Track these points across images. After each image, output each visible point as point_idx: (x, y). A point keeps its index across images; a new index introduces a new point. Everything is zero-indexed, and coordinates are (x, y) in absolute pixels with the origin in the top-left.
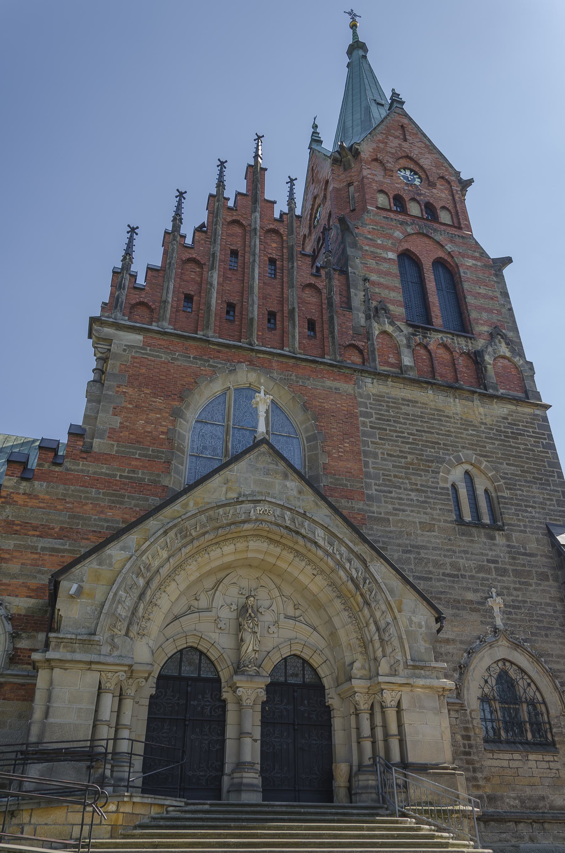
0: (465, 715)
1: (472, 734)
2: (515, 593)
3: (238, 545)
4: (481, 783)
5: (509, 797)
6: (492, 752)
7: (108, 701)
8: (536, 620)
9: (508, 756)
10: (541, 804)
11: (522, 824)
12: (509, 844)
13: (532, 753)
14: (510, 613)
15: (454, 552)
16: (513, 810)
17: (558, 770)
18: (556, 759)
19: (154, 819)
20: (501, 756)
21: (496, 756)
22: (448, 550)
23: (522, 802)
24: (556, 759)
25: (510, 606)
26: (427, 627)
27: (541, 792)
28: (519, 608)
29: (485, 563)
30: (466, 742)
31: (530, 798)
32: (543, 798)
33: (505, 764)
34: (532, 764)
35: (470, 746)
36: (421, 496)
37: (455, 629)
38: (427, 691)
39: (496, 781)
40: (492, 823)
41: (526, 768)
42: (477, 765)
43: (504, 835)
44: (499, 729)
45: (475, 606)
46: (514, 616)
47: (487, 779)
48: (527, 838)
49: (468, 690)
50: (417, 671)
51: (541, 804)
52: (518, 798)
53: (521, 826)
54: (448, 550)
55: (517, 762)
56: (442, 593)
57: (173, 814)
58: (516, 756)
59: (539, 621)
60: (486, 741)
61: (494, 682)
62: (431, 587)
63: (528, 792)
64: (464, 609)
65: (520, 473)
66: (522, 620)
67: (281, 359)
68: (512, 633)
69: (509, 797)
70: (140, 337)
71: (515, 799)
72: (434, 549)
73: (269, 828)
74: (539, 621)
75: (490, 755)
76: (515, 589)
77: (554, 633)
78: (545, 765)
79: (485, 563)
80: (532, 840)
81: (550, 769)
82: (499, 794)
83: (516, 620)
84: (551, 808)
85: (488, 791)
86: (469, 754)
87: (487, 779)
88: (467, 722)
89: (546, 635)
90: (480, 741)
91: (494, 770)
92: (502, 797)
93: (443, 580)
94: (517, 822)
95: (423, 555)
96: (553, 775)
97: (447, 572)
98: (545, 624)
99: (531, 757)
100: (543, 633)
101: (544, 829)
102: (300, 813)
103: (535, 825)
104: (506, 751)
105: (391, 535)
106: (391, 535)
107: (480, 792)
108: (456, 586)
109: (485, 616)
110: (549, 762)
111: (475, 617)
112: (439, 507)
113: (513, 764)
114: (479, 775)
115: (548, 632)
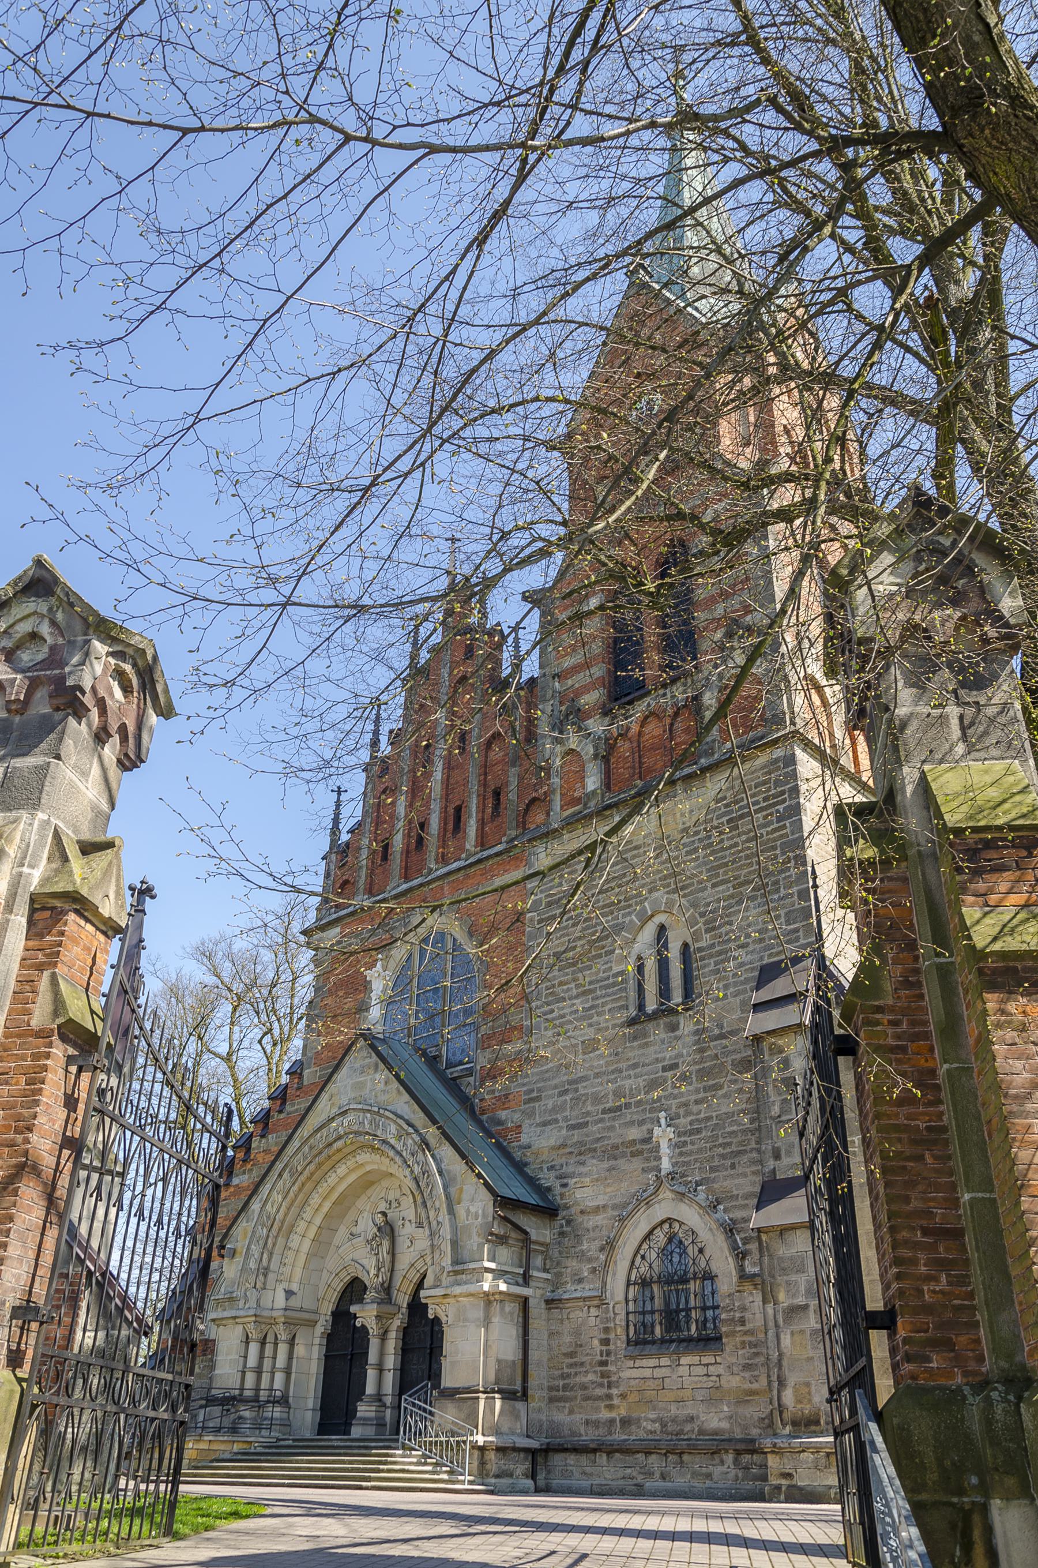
0: (607, 1311)
1: (612, 1336)
2: (695, 1108)
3: (349, 1163)
4: (616, 1401)
5: (647, 1419)
6: (633, 1358)
7: (254, 1348)
8: (720, 1145)
9: (652, 1362)
10: (688, 1427)
11: (654, 1456)
12: (635, 1481)
13: (684, 1354)
14: (685, 1143)
15: (621, 1071)
16: (650, 1437)
17: (719, 1376)
18: (719, 1359)
19: (236, 1454)
20: (645, 1363)
21: (638, 1363)
22: (613, 1072)
23: (664, 1425)
24: (719, 1359)
25: (685, 1133)
26: (484, 1216)
27: (690, 1410)
28: (699, 1131)
29: (660, 1074)
30: (604, 1348)
31: (674, 1420)
32: (691, 1419)
33: (648, 1373)
34: (683, 1371)
35: (608, 1353)
36: (587, 1001)
37: (608, 1190)
38: (472, 1299)
39: (633, 1398)
40: (617, 1455)
41: (674, 1377)
42: (614, 1378)
43: (629, 1471)
44: (653, 1326)
45: (638, 1146)
46: (690, 1147)
47: (623, 1396)
48: (657, 1475)
49: (614, 1274)
50: (459, 1277)
51: (688, 1427)
52: (660, 1420)
53: (653, 1458)
54: (613, 1072)
55: (664, 1370)
56: (598, 1140)
57: (259, 1450)
58: (665, 1361)
59: (725, 1145)
60: (629, 1342)
61: (654, 1255)
62: (587, 1135)
63: (674, 1410)
64: (623, 1155)
65: (732, 891)
66: (700, 1151)
67: (451, 878)
68: (683, 1176)
69: (647, 1419)
70: (338, 930)
71: (653, 1421)
72: (597, 1075)
73: (297, 1462)
74: (725, 1145)
75: (631, 1363)
76: (697, 1102)
77: (745, 1158)
78: (703, 1371)
79: (660, 1074)
80: (663, 1477)
81: (707, 1375)
82: (635, 1415)
83: (691, 1153)
84: (701, 1432)
85: (623, 1412)
86: (603, 1363)
87: (623, 1396)
88: (608, 1320)
89: (733, 1166)
90: (621, 1344)
91: (633, 1383)
92: (639, 1420)
93: (602, 1120)
94: (648, 1453)
95: (582, 1091)
96: (711, 1384)
97: (608, 1106)
98: (734, 1148)
99: (684, 1360)
100: (728, 1162)
101: (682, 1462)
102: (366, 1448)
103: (671, 1457)
104: (650, 1356)
105: (547, 1075)
106: (547, 1075)
107: (613, 1415)
108: (616, 1124)
109: (648, 1160)
110: (707, 1365)
111: (637, 1163)
112: (607, 1008)
113: (659, 1373)
114: (614, 1391)
115: (736, 1160)
